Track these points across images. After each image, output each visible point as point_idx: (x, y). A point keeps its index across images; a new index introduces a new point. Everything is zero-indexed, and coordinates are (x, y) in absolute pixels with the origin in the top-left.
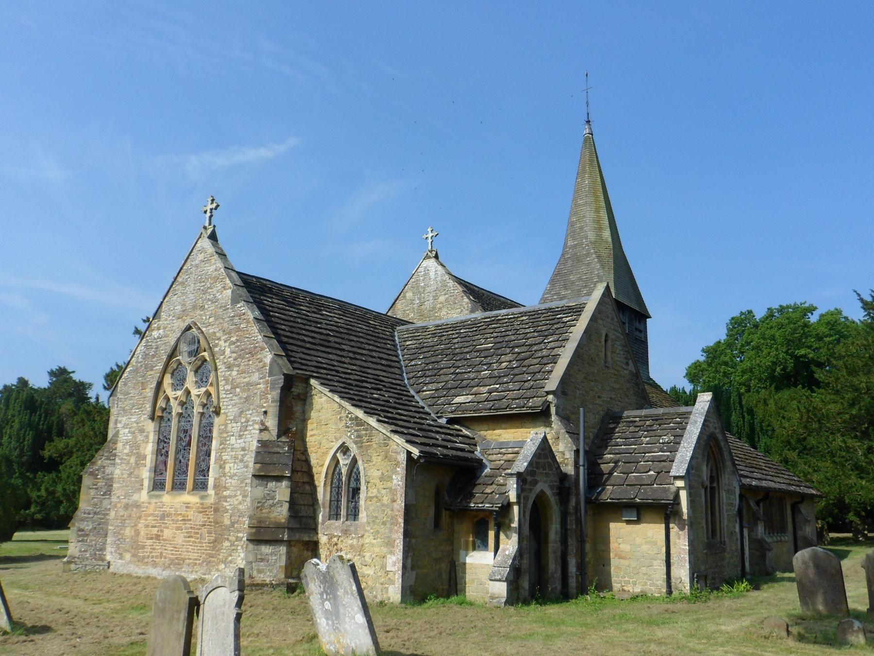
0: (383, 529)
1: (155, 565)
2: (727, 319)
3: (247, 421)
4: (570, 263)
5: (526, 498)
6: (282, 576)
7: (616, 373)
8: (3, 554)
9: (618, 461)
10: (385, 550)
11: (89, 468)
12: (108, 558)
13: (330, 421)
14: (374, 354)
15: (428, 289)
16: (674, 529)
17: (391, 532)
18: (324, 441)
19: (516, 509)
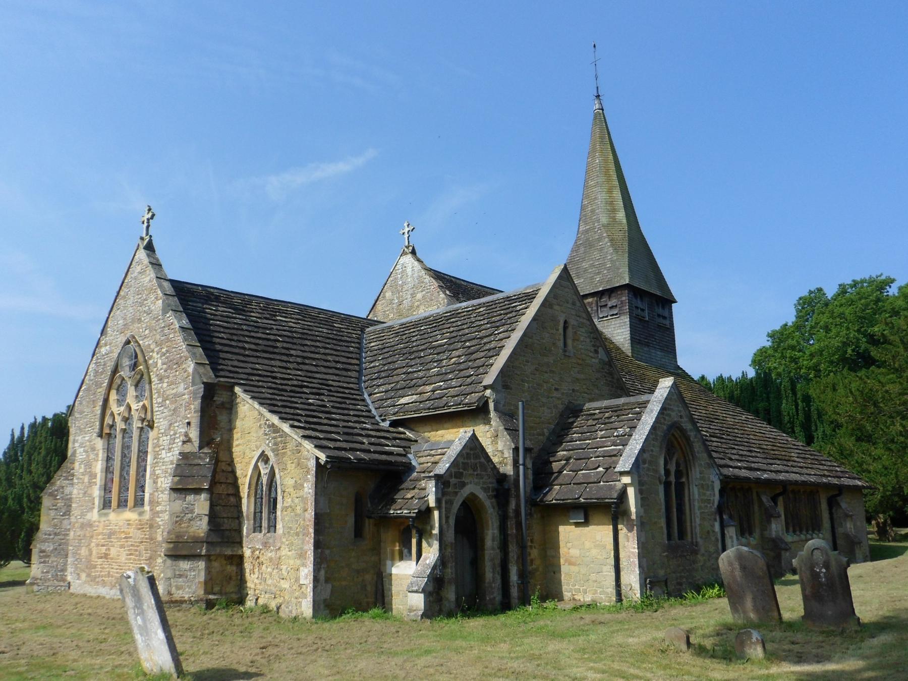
0: (297, 541)
1: (104, 584)
2: (795, 301)
3: (175, 434)
4: (582, 249)
5: (450, 503)
6: (201, 592)
7: (580, 362)
8: (4, 578)
9: (570, 458)
10: (298, 562)
11: (50, 489)
12: (69, 578)
13: (253, 426)
14: (329, 358)
15: (406, 287)
16: (623, 530)
17: (303, 543)
18: (247, 451)
19: (436, 514)
